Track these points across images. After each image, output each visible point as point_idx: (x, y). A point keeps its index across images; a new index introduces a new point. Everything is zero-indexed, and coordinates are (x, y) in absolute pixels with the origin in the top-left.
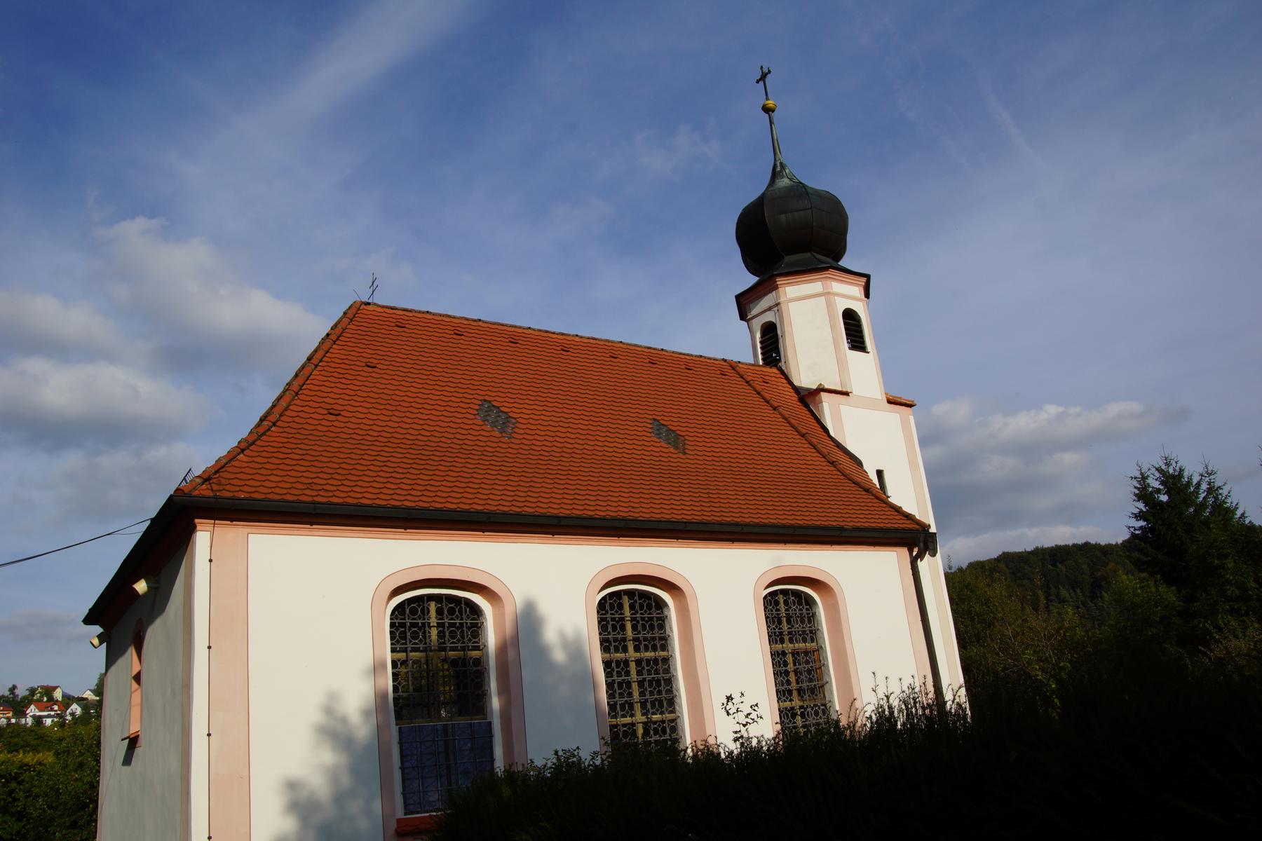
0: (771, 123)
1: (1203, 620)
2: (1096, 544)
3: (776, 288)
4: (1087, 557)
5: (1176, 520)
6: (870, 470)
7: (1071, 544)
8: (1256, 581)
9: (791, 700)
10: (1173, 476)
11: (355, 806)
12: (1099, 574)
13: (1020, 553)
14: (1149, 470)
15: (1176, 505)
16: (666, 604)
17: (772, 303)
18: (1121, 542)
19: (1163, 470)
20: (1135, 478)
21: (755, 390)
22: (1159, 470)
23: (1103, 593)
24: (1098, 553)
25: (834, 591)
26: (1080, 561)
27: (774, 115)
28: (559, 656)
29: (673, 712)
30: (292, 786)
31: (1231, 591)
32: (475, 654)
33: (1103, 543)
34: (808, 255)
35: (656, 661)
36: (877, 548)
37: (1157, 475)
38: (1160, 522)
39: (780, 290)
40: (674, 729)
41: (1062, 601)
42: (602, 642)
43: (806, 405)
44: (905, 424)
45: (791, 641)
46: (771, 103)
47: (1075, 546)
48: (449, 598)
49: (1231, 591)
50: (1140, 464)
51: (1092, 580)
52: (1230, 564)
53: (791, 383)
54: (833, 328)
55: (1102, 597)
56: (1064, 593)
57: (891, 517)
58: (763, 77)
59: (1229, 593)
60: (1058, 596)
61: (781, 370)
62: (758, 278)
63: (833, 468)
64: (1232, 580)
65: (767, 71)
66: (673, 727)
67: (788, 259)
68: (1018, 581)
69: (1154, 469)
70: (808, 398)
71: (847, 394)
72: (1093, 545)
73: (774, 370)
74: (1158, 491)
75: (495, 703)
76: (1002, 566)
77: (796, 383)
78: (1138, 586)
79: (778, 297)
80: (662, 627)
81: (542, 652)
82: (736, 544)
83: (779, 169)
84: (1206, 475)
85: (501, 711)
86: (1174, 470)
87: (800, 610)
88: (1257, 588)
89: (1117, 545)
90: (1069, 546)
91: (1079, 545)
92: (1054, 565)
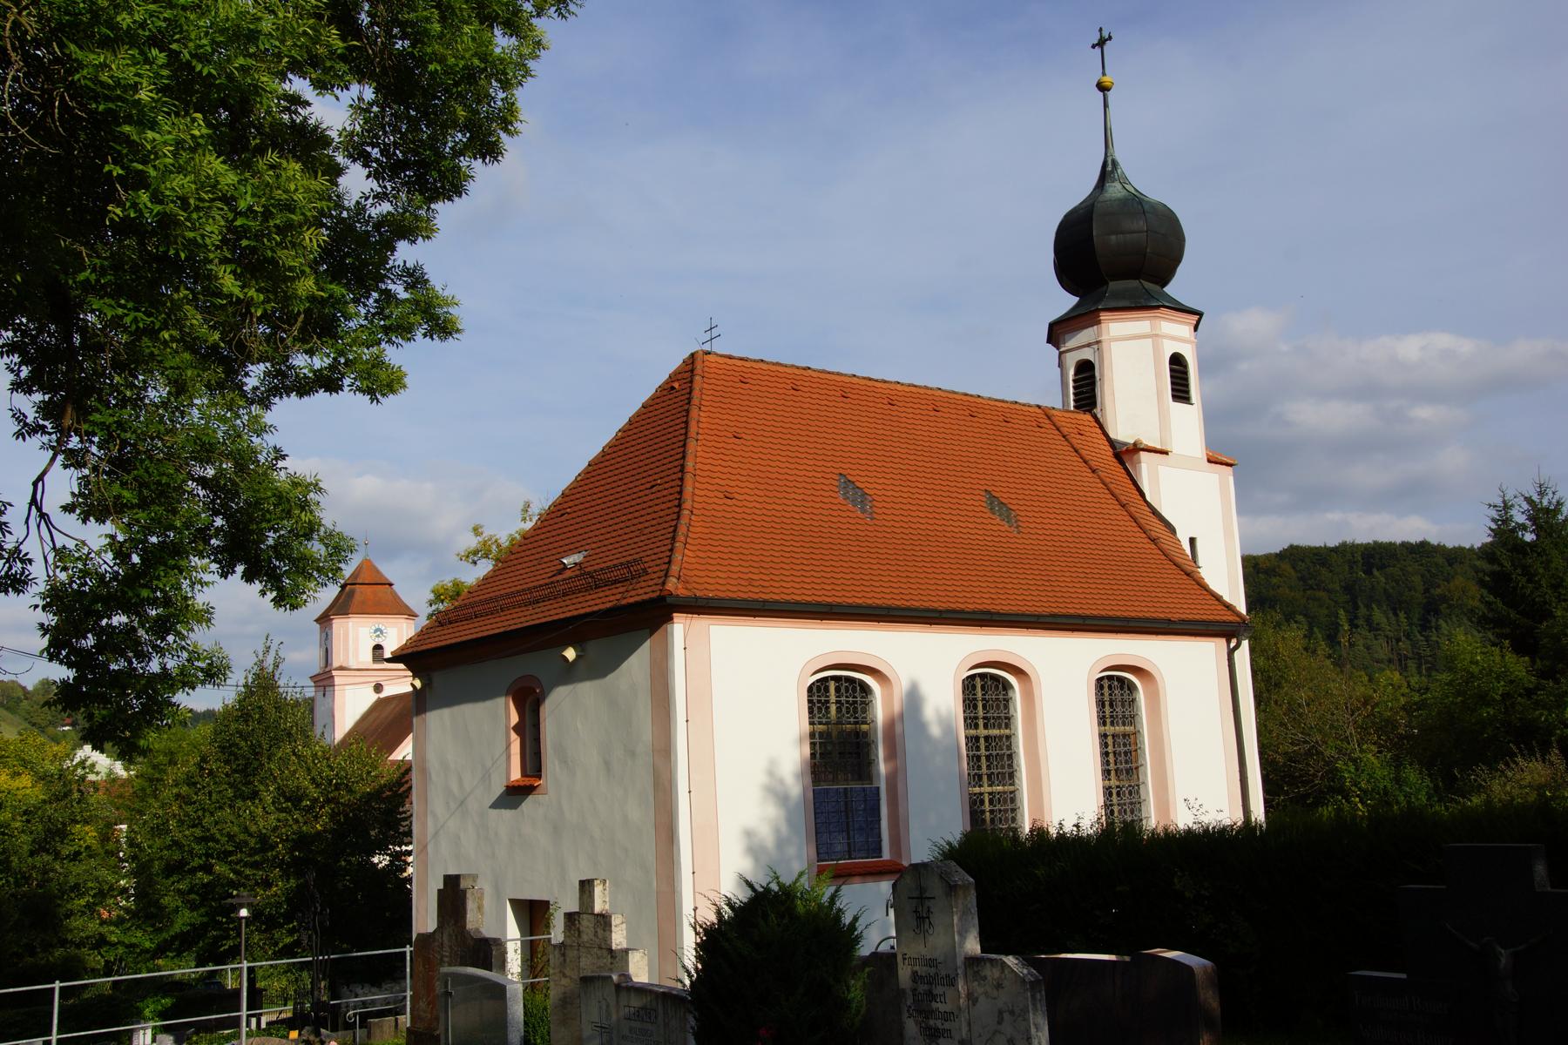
0: (1106, 105)
1: (1545, 713)
3: (1099, 322)
4: (1422, 565)
5: (1541, 571)
7: (1398, 541)
9: (1109, 780)
10: (1547, 511)
11: (791, 851)
12: (1439, 591)
13: (1316, 548)
15: (1544, 550)
16: (1011, 687)
18: (1480, 545)
19: (1533, 501)
20: (1495, 506)
21: (1073, 447)
22: (1529, 500)
23: (1441, 622)
24: (1440, 560)
26: (1410, 569)
27: (1110, 94)
28: (935, 731)
29: (1012, 784)
30: (749, 834)
32: (864, 727)
33: (1450, 544)
34: (1133, 283)
35: (1001, 737)
36: (1198, 638)
37: (1525, 506)
38: (1519, 571)
39: (1103, 325)
40: (1013, 800)
41: (1373, 627)
43: (1122, 463)
45: (1112, 724)
46: (1107, 80)
47: (1405, 545)
48: (848, 679)
50: (1504, 488)
51: (1425, 601)
53: (1105, 434)
54: (1158, 375)
55: (1438, 628)
56: (1378, 616)
57: (1212, 607)
58: (1101, 43)
60: (1369, 620)
62: (1074, 300)
66: (1012, 798)
67: (1114, 285)
68: (1309, 592)
69: (1522, 499)
70: (1125, 454)
71: (1165, 453)
72: (1433, 547)
73: (1088, 417)
74: (1524, 527)
75: (883, 768)
76: (1286, 567)
77: (1112, 436)
78: (1479, 651)
79: (1099, 334)
80: (1006, 707)
81: (922, 727)
82: (1075, 633)
83: (1109, 168)
85: (887, 778)
86: (1550, 503)
87: (1122, 695)
89: (1471, 549)
90: (1394, 544)
92: (1369, 572)
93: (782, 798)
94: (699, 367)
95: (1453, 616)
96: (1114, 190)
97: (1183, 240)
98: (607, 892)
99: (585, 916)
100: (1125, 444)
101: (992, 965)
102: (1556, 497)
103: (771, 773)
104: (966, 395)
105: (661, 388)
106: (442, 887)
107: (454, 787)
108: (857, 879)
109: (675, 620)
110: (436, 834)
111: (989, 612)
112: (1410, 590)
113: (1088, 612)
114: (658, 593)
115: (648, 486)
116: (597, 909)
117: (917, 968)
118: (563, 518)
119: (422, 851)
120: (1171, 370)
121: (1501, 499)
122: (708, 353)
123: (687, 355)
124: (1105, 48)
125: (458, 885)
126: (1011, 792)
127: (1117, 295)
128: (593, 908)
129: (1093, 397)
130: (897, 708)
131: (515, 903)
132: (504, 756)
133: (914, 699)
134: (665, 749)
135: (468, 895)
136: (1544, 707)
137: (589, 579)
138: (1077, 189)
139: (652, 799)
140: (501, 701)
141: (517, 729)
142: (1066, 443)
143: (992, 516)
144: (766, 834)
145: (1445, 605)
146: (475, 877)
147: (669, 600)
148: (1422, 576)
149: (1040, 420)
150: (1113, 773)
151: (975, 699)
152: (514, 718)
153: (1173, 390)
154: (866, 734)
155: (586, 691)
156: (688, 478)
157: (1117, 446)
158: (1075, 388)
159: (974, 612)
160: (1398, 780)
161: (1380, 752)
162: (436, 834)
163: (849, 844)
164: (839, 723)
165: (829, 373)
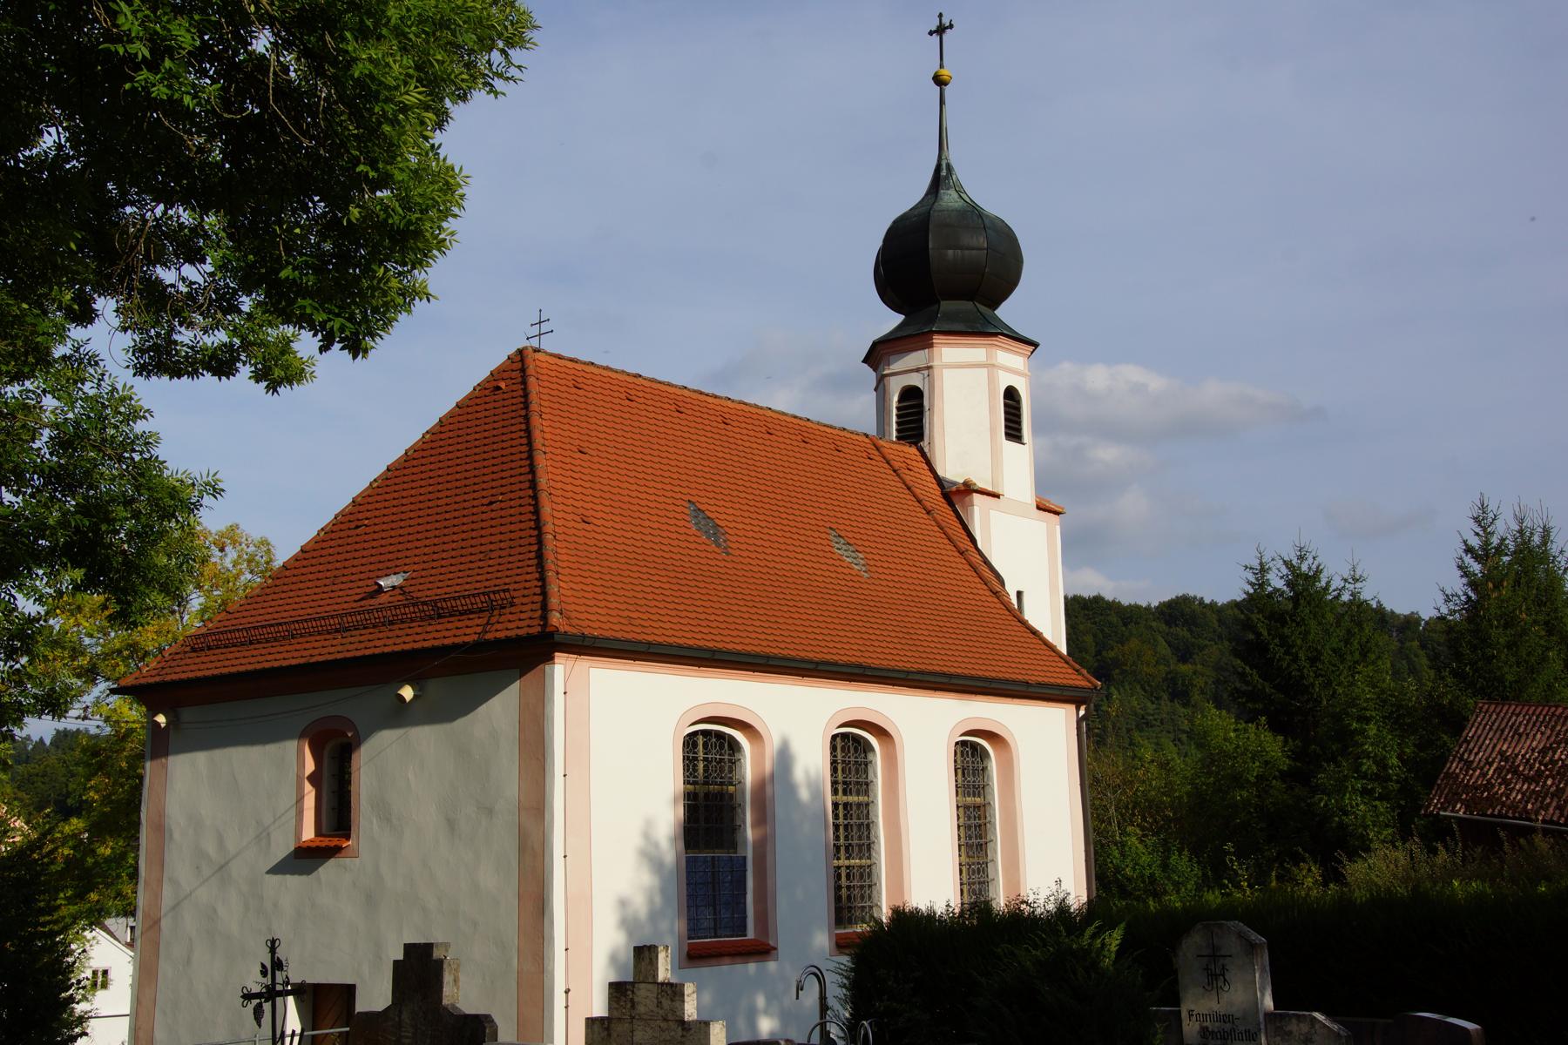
0: (942, 102)
1: (1325, 798)
2: (1114, 601)
3: (931, 346)
4: (1095, 623)
5: (1299, 642)
6: (1011, 590)
8: (1399, 757)
10: (1307, 577)
11: (664, 925)
12: (1112, 654)
14: (1273, 560)
16: (872, 749)
18: (1157, 604)
19: (1292, 564)
20: (1251, 568)
21: (904, 483)
22: (1287, 564)
23: (1113, 689)
24: (1114, 619)
25: (1009, 745)
27: (947, 89)
28: (804, 794)
29: (869, 858)
30: (623, 903)
31: (1368, 765)
37: (1285, 571)
38: (1277, 641)
42: (834, 783)
43: (951, 504)
44: (1050, 535)
46: (945, 72)
48: (720, 735)
49: (1368, 765)
51: (1096, 664)
52: (1372, 730)
54: (992, 409)
58: (941, 30)
59: (1364, 768)
61: (923, 455)
62: (901, 318)
63: (996, 600)
64: (1370, 752)
65: (948, 24)
67: (946, 306)
69: (1281, 562)
70: (957, 495)
71: (997, 496)
73: (913, 450)
77: (940, 473)
78: (1232, 727)
79: (931, 358)
80: (866, 772)
81: (791, 788)
82: (937, 692)
83: (944, 173)
84: (1351, 581)
85: (754, 842)
86: (1310, 568)
88: (1399, 766)
89: (1148, 608)
91: (1085, 599)
93: (656, 864)
94: (531, 369)
95: (1126, 684)
96: (949, 199)
97: (1021, 261)
98: (669, 959)
99: (642, 986)
100: (954, 483)
101: (1299, 1021)
102: (1316, 563)
103: (647, 835)
104: (795, 417)
105: (481, 387)
106: (401, 957)
107: (210, 847)
108: (727, 960)
109: (556, 660)
111: (860, 666)
112: (1080, 652)
113: (952, 670)
114: (539, 629)
115: (485, 501)
116: (661, 978)
117: (1208, 1024)
118: (359, 531)
119: (151, 927)
120: (1006, 405)
121: (1258, 561)
122: (537, 351)
123: (512, 350)
124: (945, 37)
125: (431, 954)
126: (869, 866)
127: (950, 317)
128: (655, 975)
129: (921, 428)
130: (768, 767)
132: (293, 812)
133: (785, 758)
134: (536, 806)
135: (445, 966)
136: (1323, 792)
137: (412, 607)
138: (909, 193)
140: (291, 746)
141: (313, 779)
142: (897, 479)
143: (716, 550)
144: (640, 905)
145: (1117, 671)
146: (446, 946)
147: (557, 638)
148: (1095, 636)
149: (869, 451)
150: (842, 849)
151: (696, 759)
152: (310, 766)
153: (1006, 427)
154: (731, 796)
155: (425, 737)
156: (543, 496)
157: (946, 484)
158: (898, 416)
159: (846, 665)
160: (1165, 866)
161: (1144, 836)
163: (715, 920)
164: (706, 783)
165: (660, 382)
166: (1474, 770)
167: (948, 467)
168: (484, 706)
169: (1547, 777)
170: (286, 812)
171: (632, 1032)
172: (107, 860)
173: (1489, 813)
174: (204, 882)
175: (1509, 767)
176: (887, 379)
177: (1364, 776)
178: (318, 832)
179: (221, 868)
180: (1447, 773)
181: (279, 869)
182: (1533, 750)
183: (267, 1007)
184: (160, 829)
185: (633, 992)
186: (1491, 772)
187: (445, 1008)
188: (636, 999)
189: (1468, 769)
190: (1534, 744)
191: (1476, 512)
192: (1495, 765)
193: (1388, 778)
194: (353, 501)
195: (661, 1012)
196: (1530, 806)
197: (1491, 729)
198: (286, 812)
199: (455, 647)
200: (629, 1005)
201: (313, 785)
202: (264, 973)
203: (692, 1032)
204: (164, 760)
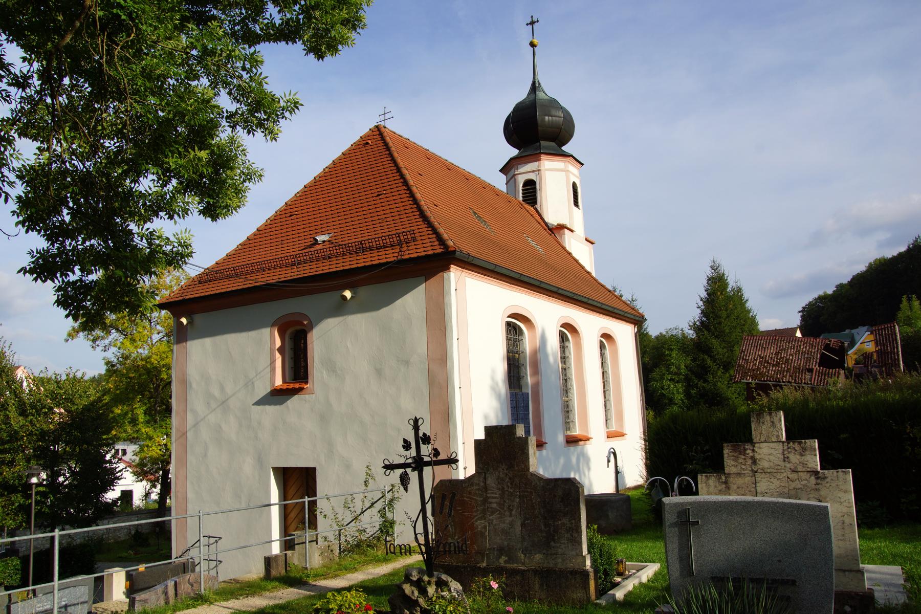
3: (539, 160)
17: (536, 168)
31: (673, 369)
46: (536, 41)
49: (673, 369)
54: (568, 191)
58: (532, 23)
65: (536, 20)
73: (532, 208)
75: (530, 380)
81: (546, 356)
83: (537, 85)
93: (499, 396)
100: (553, 225)
107: (216, 392)
110: (196, 425)
118: (292, 217)
119: (181, 437)
123: (372, 126)
126: (567, 401)
131: (276, 470)
132: (269, 369)
136: (655, 381)
137: (337, 249)
138: (521, 94)
139: (426, 393)
140: (266, 331)
141: (279, 350)
152: (278, 343)
155: (359, 322)
158: (523, 194)
162: (196, 425)
166: (750, 363)
167: (549, 217)
168: (400, 300)
169: (782, 364)
170: (264, 370)
171: (756, 484)
172: (119, 415)
173: (763, 379)
174: (212, 411)
175: (765, 362)
176: (516, 177)
177: (671, 373)
178: (284, 381)
179: (223, 402)
180: (739, 364)
181: (259, 403)
182: (772, 354)
183: (413, 476)
184: (184, 382)
185: (753, 451)
186: (757, 363)
187: (533, 475)
188: (757, 456)
189: (747, 363)
190: (772, 351)
191: (711, 264)
192: (758, 361)
193: (680, 374)
194: (286, 204)
195: (788, 465)
196: (778, 376)
197: (751, 346)
198: (264, 370)
199: (380, 265)
200: (749, 462)
201: (280, 354)
202: (407, 446)
203: (827, 480)
204: (184, 344)
